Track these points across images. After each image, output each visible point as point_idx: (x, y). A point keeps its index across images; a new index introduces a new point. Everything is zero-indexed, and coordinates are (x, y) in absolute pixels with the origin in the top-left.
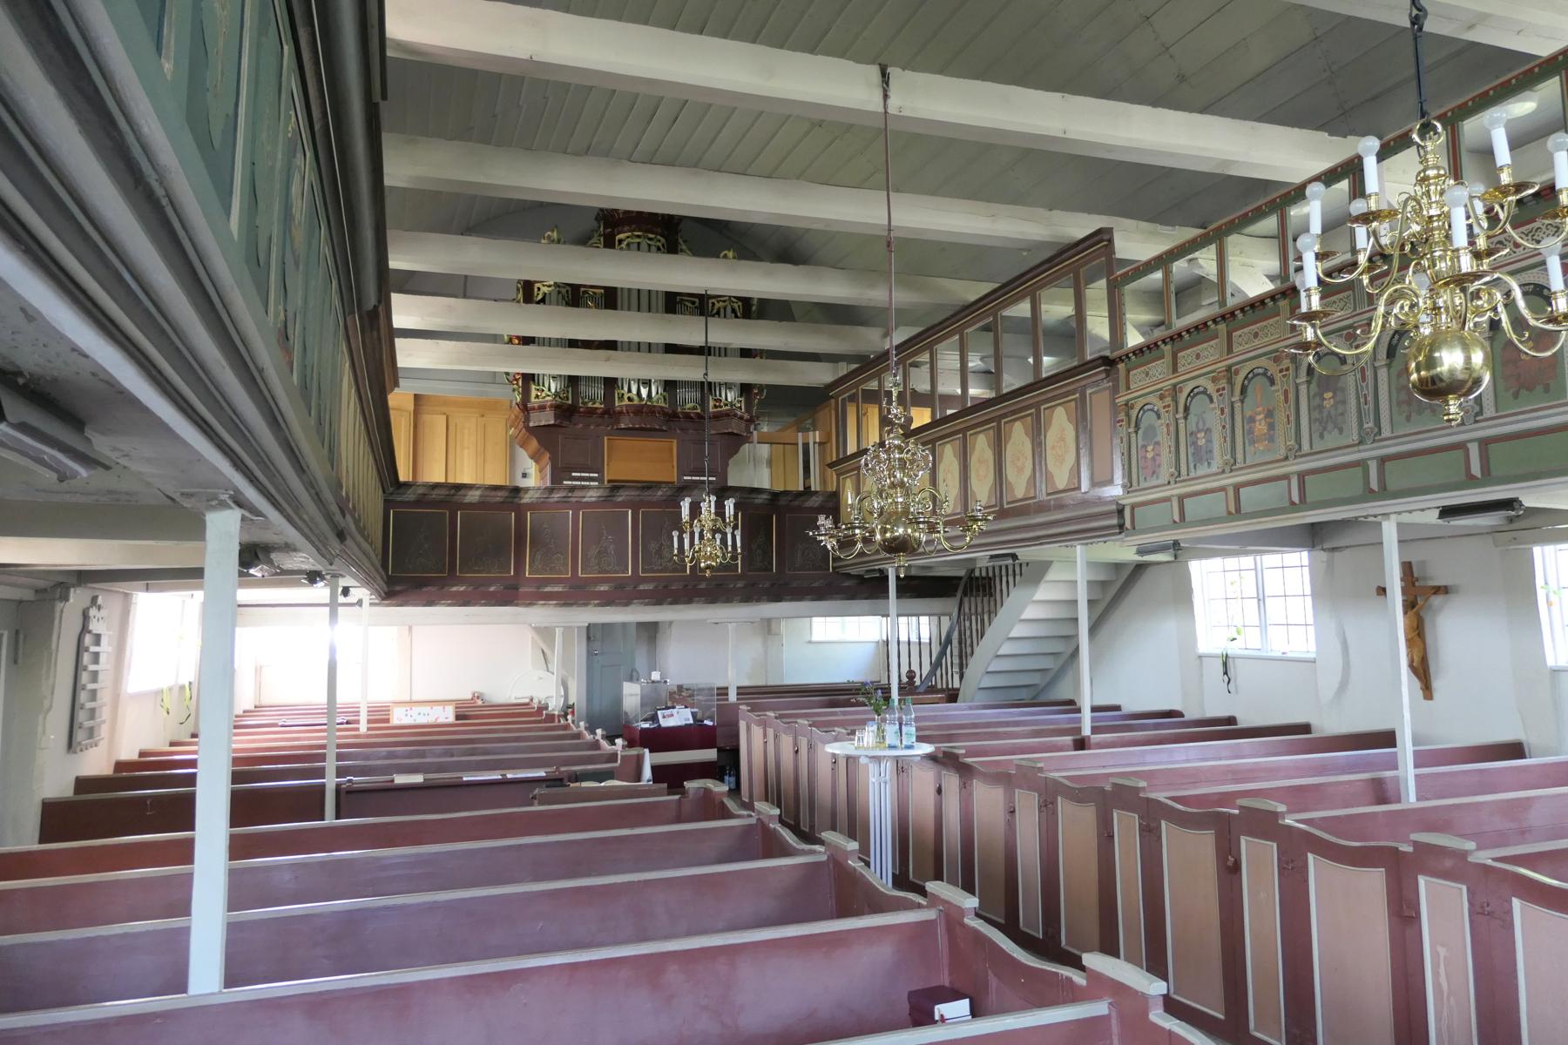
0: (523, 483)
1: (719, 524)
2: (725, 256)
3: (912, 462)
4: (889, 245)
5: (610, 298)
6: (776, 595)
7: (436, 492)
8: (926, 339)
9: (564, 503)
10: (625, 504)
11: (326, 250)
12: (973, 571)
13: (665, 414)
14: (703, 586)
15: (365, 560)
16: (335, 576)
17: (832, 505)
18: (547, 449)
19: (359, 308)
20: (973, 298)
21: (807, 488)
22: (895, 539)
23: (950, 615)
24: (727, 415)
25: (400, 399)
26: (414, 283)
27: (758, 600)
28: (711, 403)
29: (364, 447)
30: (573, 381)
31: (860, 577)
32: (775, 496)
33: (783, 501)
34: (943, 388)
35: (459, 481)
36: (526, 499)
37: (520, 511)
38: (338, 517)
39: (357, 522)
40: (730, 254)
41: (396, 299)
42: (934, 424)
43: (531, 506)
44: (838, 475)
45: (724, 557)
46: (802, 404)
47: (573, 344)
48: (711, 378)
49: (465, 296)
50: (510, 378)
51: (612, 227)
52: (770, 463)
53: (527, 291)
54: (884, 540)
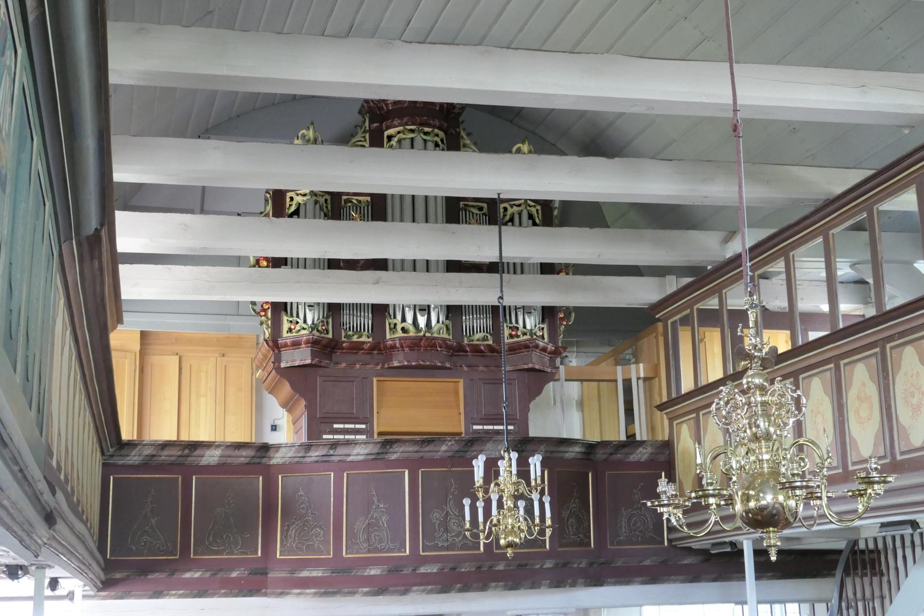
0: (273, 439)
1: (523, 488)
2: (519, 151)
3: (780, 406)
4: (735, 129)
5: (378, 208)
6: (596, 579)
7: (166, 452)
8: (779, 243)
9: (324, 462)
10: (402, 463)
11: (39, 165)
12: (856, 542)
13: (448, 347)
14: (501, 567)
15: (81, 549)
16: (42, 567)
17: (664, 459)
18: (303, 395)
19: (78, 233)
20: (839, 190)
21: (631, 436)
22: (762, 509)
23: (827, 602)
24: (526, 346)
25: (123, 338)
26: (141, 198)
27: (573, 585)
28: (507, 332)
29: (80, 401)
30: (334, 309)
31: (704, 552)
32: (591, 448)
33: (600, 455)
34: (804, 305)
35: (194, 438)
36: (277, 459)
37: (269, 473)
38: (47, 496)
39: (68, 497)
40: (525, 148)
41: (122, 218)
42: (795, 351)
43: (284, 468)
44: (671, 420)
45: (530, 532)
46: (621, 329)
47: (333, 264)
48: (507, 302)
49: (203, 211)
50: (258, 309)
51: (380, 121)
52: (581, 405)
53: (279, 204)
54: (747, 512)
